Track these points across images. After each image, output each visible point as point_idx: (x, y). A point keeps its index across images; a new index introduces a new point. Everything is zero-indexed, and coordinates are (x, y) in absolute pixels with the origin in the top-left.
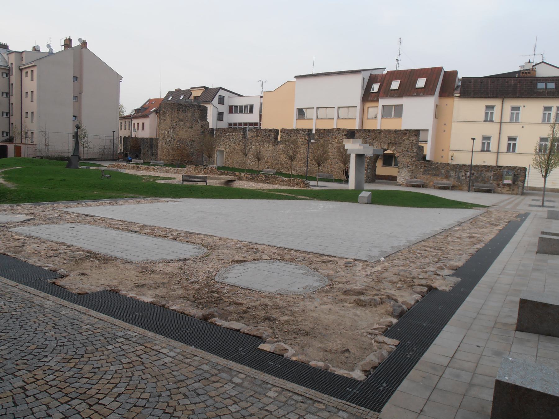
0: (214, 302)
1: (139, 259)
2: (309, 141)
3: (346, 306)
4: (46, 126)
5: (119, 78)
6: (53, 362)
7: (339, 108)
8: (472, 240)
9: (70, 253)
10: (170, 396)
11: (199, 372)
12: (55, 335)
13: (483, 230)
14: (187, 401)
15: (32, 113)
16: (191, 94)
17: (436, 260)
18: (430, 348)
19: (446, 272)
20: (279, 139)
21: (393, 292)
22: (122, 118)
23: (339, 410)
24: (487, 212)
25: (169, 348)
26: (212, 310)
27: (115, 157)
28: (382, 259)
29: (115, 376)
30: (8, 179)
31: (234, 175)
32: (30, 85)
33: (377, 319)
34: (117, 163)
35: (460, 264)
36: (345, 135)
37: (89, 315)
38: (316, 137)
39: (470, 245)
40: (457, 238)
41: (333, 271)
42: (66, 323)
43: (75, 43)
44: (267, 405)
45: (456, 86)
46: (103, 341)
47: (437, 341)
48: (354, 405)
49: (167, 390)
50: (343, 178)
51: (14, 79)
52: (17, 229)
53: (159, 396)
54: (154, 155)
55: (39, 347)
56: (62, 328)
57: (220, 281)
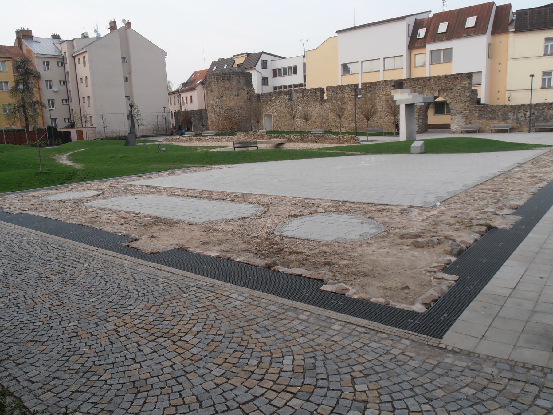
0: (275, 253)
1: (201, 221)
2: (356, 96)
3: (403, 249)
4: (102, 108)
5: (164, 54)
6: (138, 309)
7: (384, 59)
8: (534, 179)
9: (139, 220)
10: (243, 332)
11: (267, 312)
12: (136, 288)
13: (546, 169)
14: (259, 336)
15: (89, 97)
16: (234, 62)
17: (495, 201)
18: (490, 282)
19: (506, 211)
20: (325, 98)
21: (450, 233)
22: (171, 93)
23: (402, 338)
24: (550, 151)
25: (238, 294)
26: (274, 259)
27: (168, 132)
28: (438, 204)
29: (192, 318)
30: (75, 160)
31: (284, 137)
32: (83, 71)
33: (435, 258)
34: (171, 137)
35: (521, 203)
36: (393, 86)
37: (163, 270)
38: (363, 91)
39: (531, 184)
40: (517, 178)
41: (389, 218)
42: (144, 278)
43: (120, 25)
44: (333, 336)
45: (510, 21)
46: (178, 290)
47: (498, 274)
48: (416, 334)
49: (240, 327)
50: (394, 130)
51: (68, 67)
52: (90, 203)
53: (233, 333)
54: (205, 126)
55: (124, 298)
56: (141, 282)
57: (279, 234)
